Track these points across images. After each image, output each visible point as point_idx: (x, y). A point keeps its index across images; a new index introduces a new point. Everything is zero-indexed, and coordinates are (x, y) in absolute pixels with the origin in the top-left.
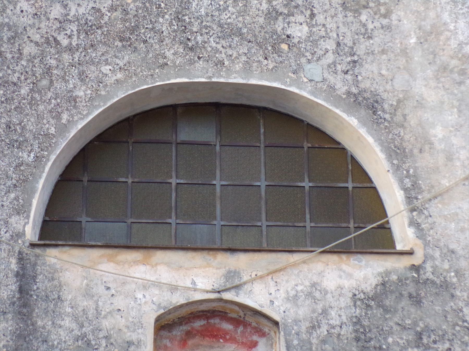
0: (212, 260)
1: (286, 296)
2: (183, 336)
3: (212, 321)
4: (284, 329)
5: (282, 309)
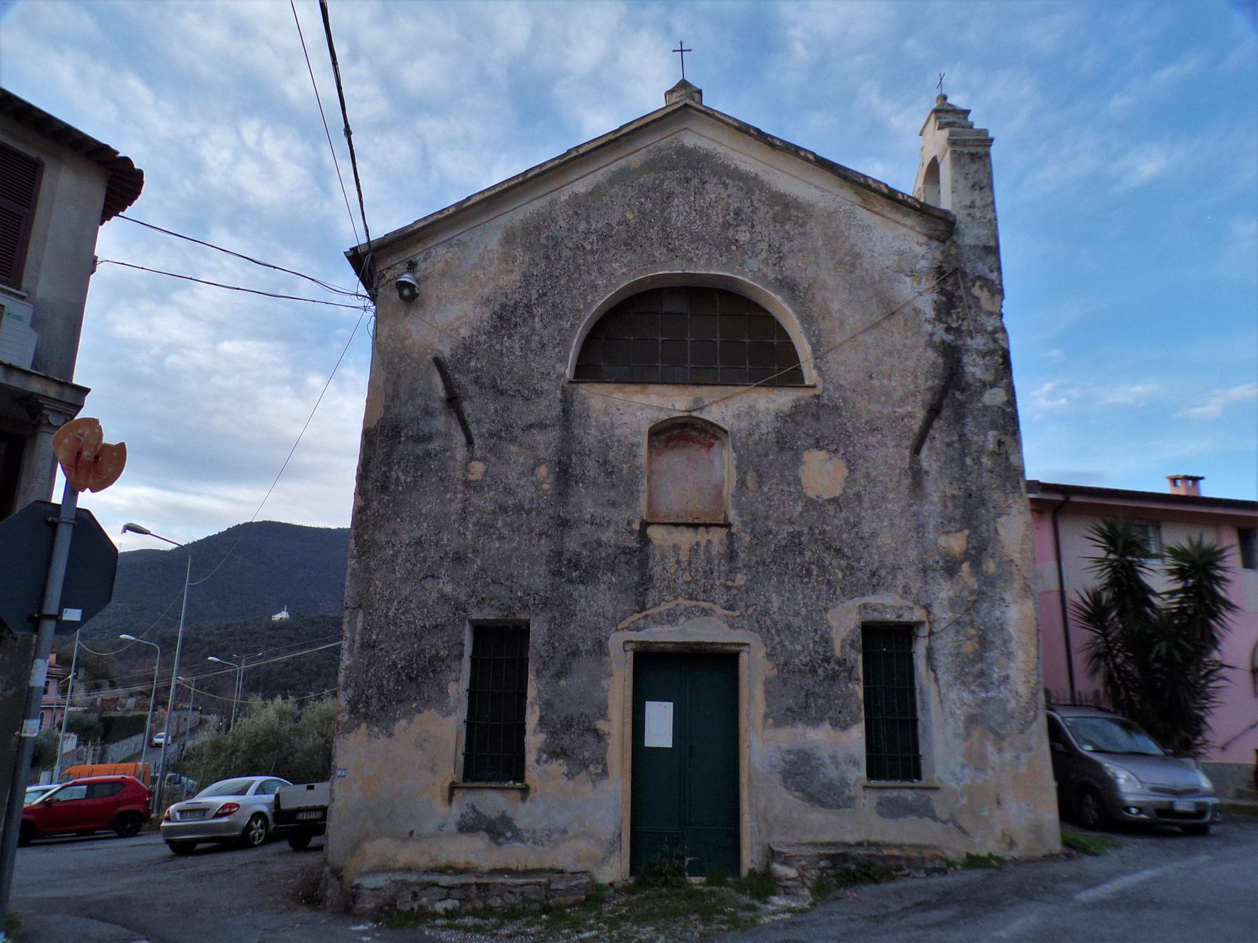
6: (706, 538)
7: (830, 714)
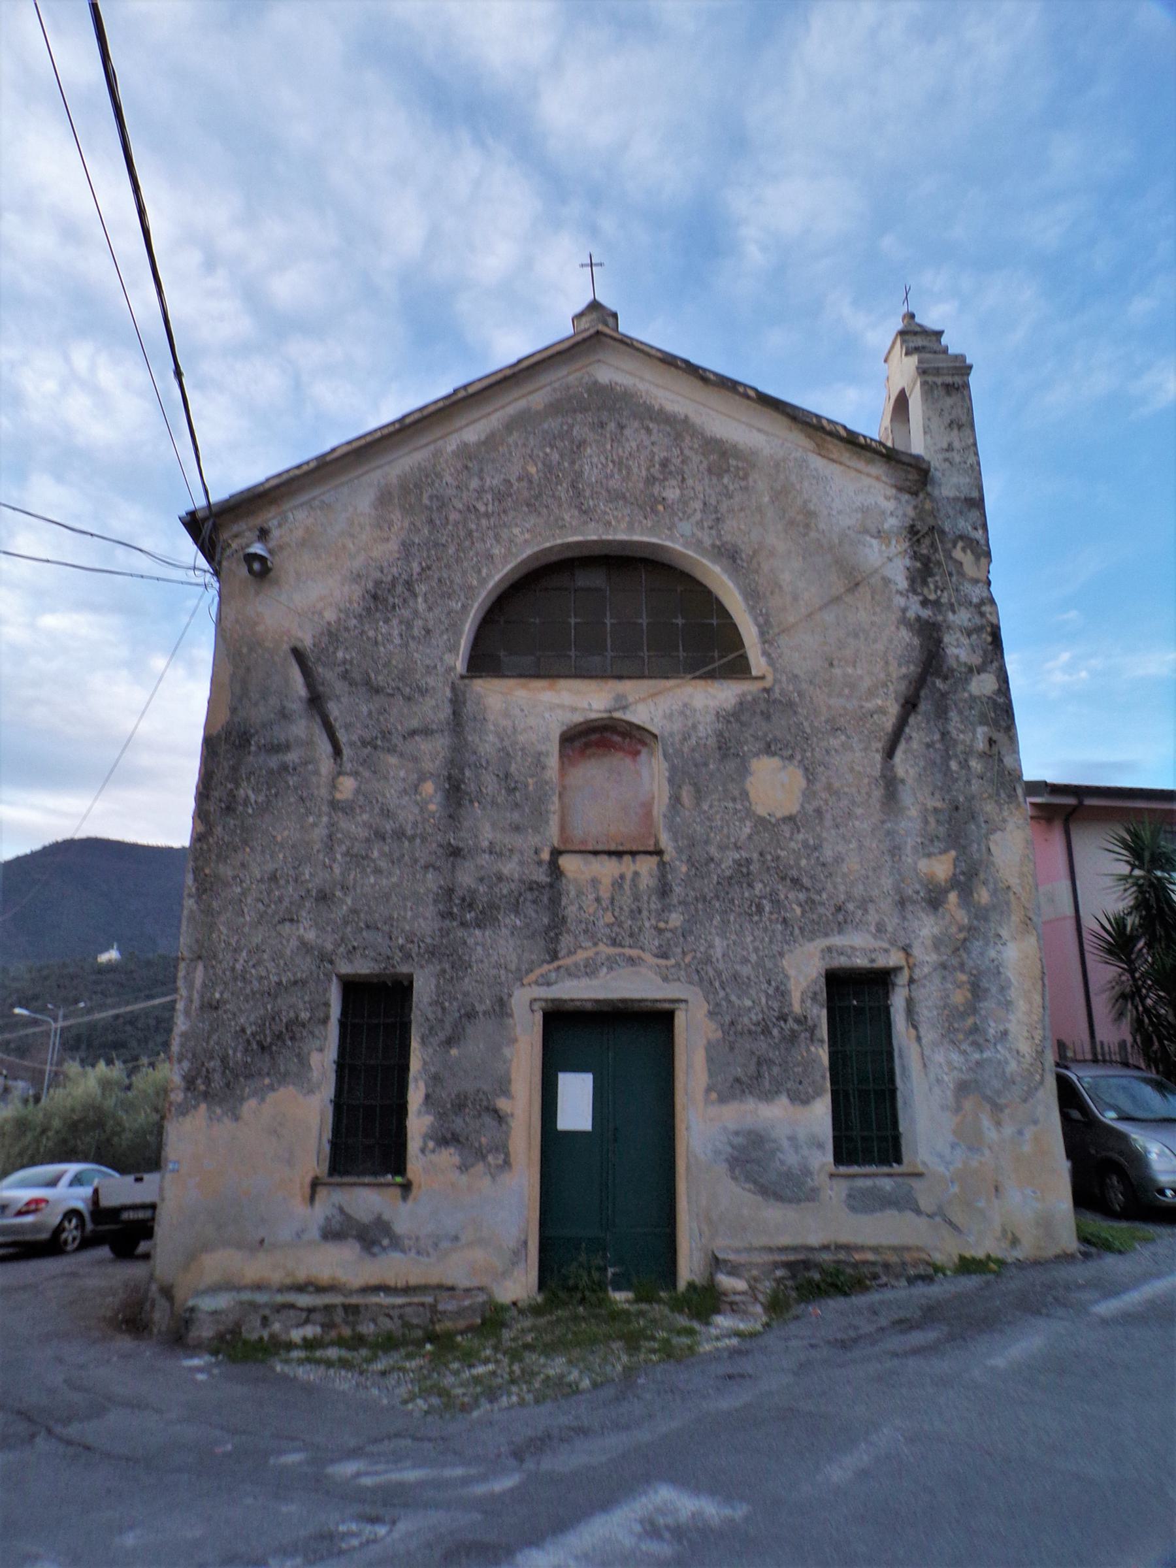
6: (632, 868)
7: (789, 1086)
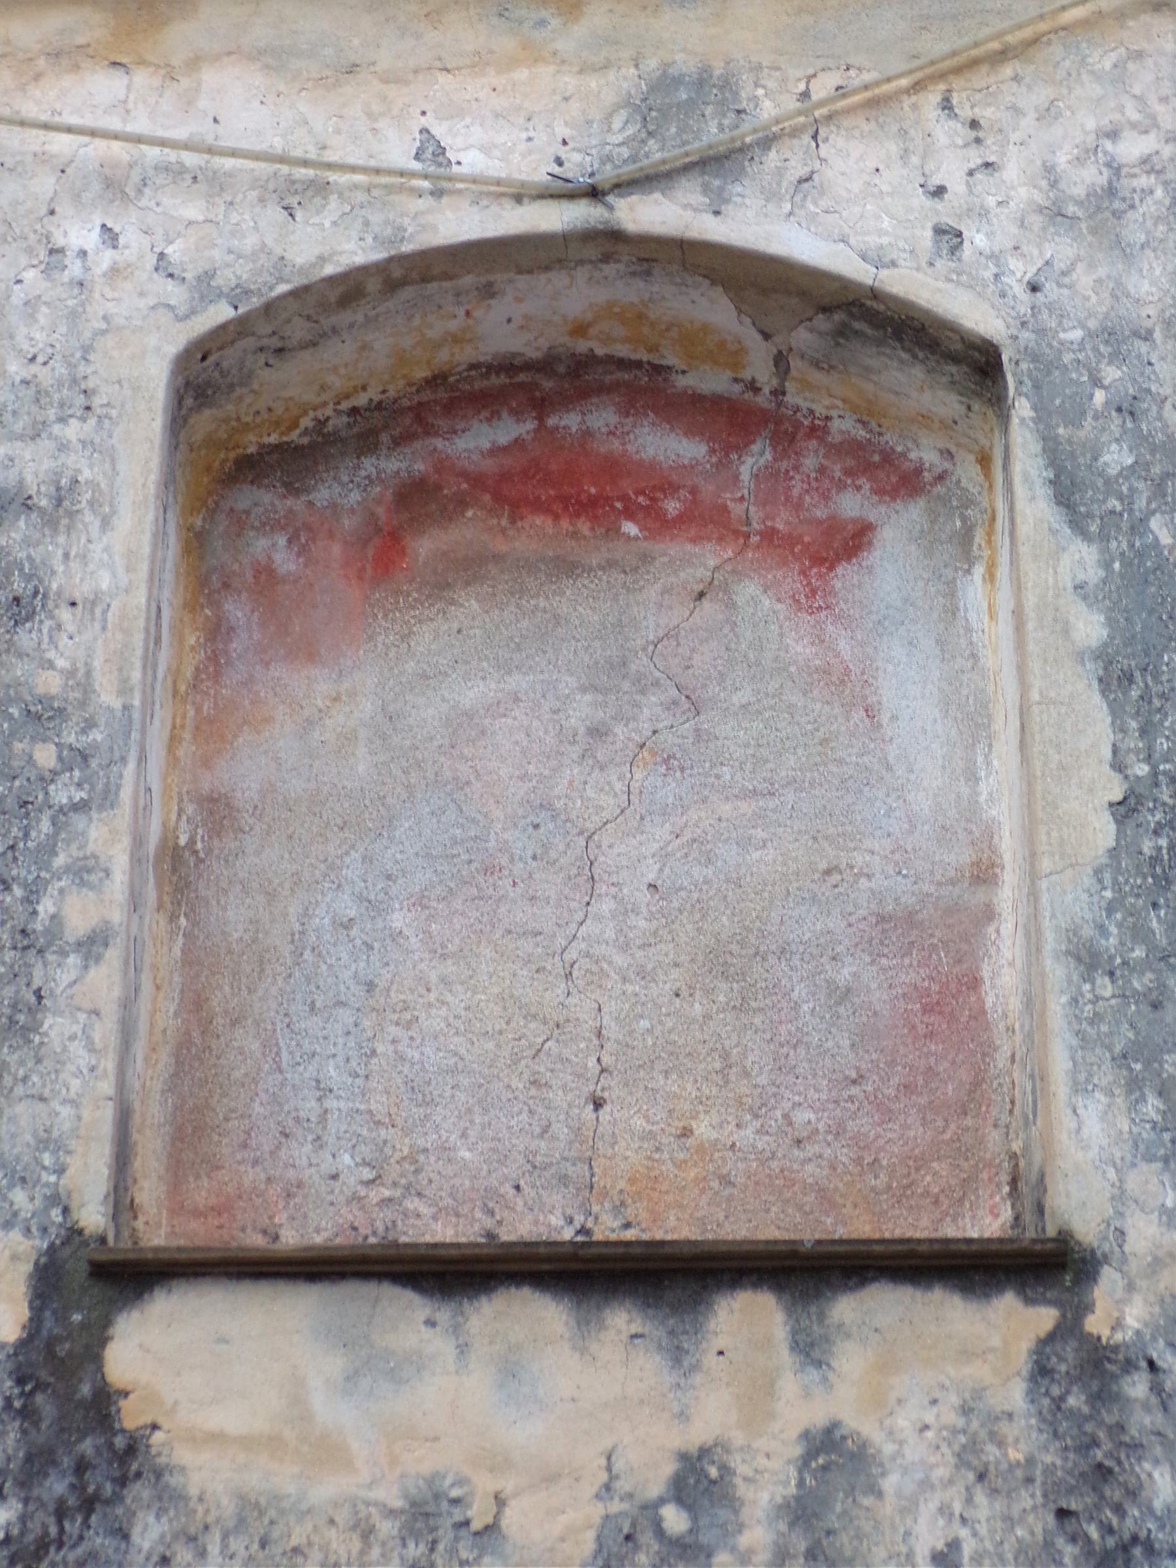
0: (555, 22)
1: (1039, 198)
2: (380, 511)
3: (570, 421)
4: (1037, 387)
5: (1019, 270)
6: (800, 1406)
